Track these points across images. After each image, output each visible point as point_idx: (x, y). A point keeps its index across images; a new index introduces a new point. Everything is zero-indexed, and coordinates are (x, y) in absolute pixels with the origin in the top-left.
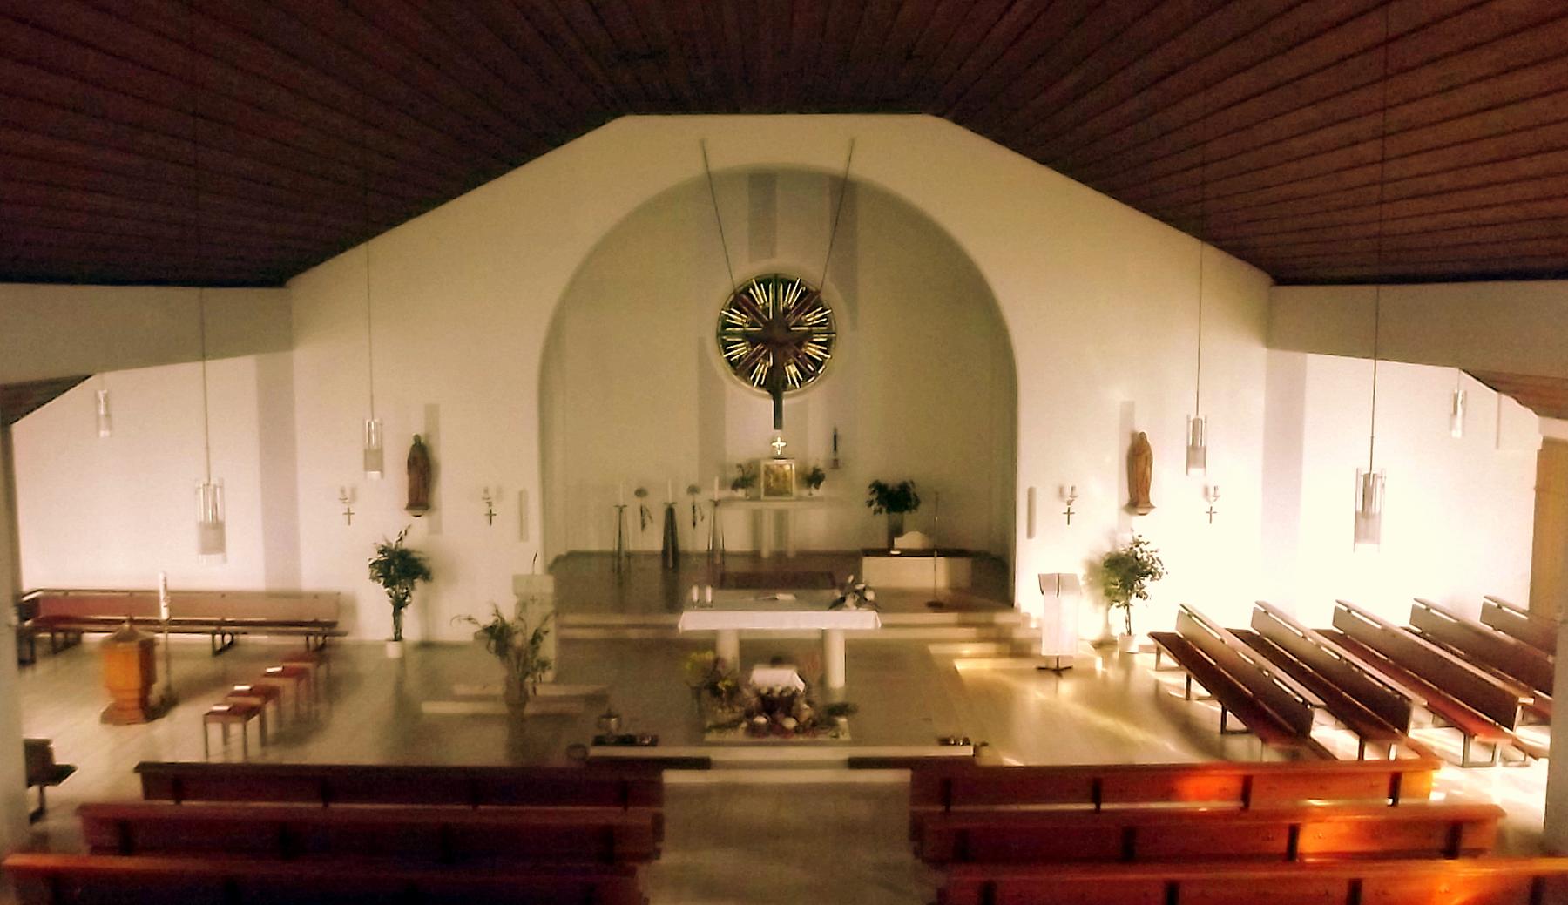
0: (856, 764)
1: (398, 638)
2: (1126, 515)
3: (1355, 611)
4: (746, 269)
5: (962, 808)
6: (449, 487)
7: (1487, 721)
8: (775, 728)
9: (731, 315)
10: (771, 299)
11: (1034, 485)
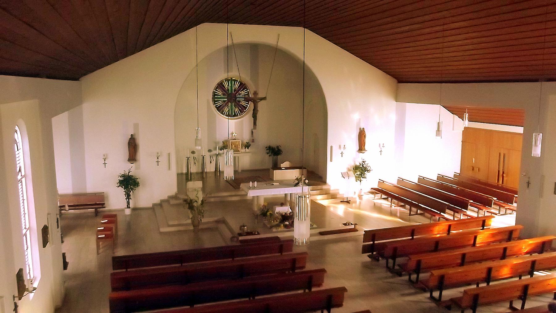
1: (128, 207)
2: (358, 153)
3: (404, 180)
4: (222, 76)
6: (142, 153)
7: (459, 209)
9: (217, 92)
11: (332, 145)
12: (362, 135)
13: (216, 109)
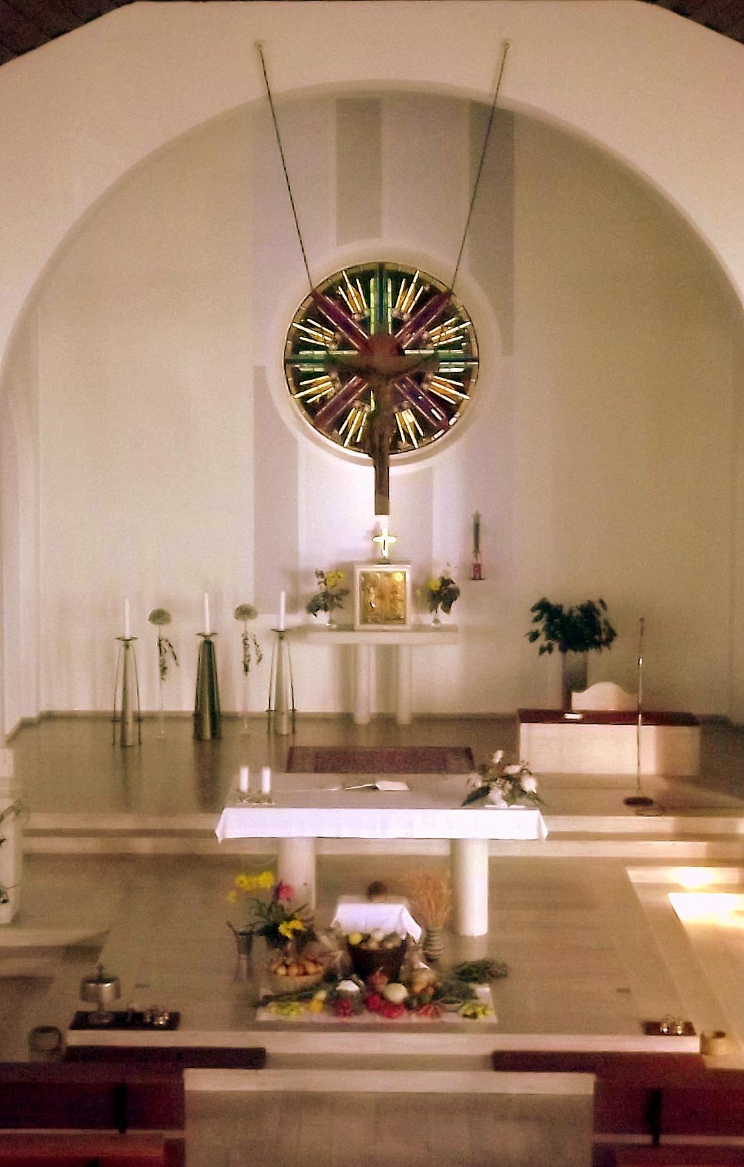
0: (504, 1062)
8: (373, 1001)
10: (372, 305)
13: (302, 414)
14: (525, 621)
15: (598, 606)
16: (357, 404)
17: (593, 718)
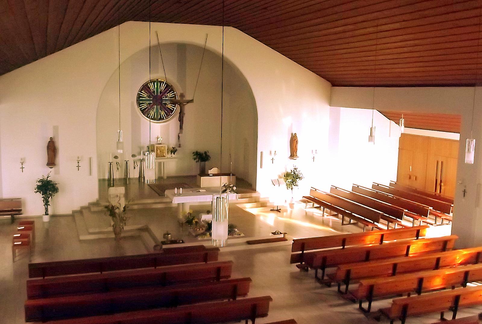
0: (249, 243)
1: (47, 214)
5: (210, 262)
12: (293, 141)
14: (192, 156)
15: (207, 152)
16: (148, 95)
17: (214, 175)
